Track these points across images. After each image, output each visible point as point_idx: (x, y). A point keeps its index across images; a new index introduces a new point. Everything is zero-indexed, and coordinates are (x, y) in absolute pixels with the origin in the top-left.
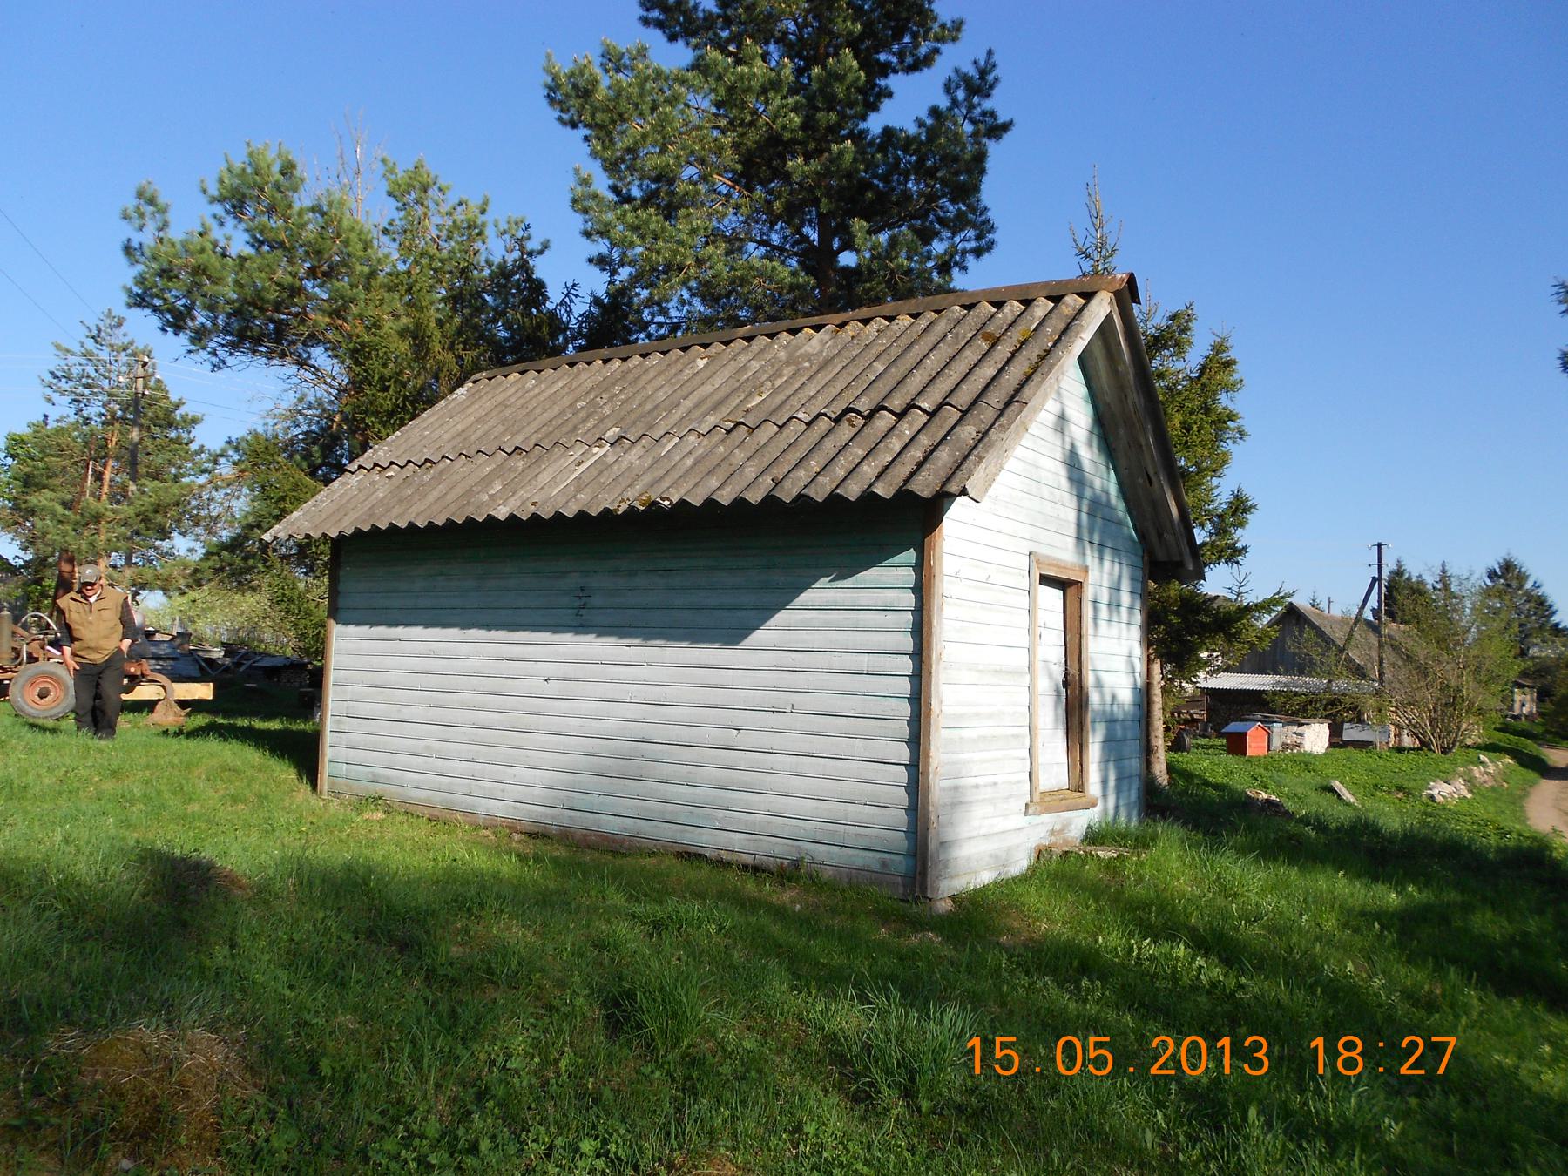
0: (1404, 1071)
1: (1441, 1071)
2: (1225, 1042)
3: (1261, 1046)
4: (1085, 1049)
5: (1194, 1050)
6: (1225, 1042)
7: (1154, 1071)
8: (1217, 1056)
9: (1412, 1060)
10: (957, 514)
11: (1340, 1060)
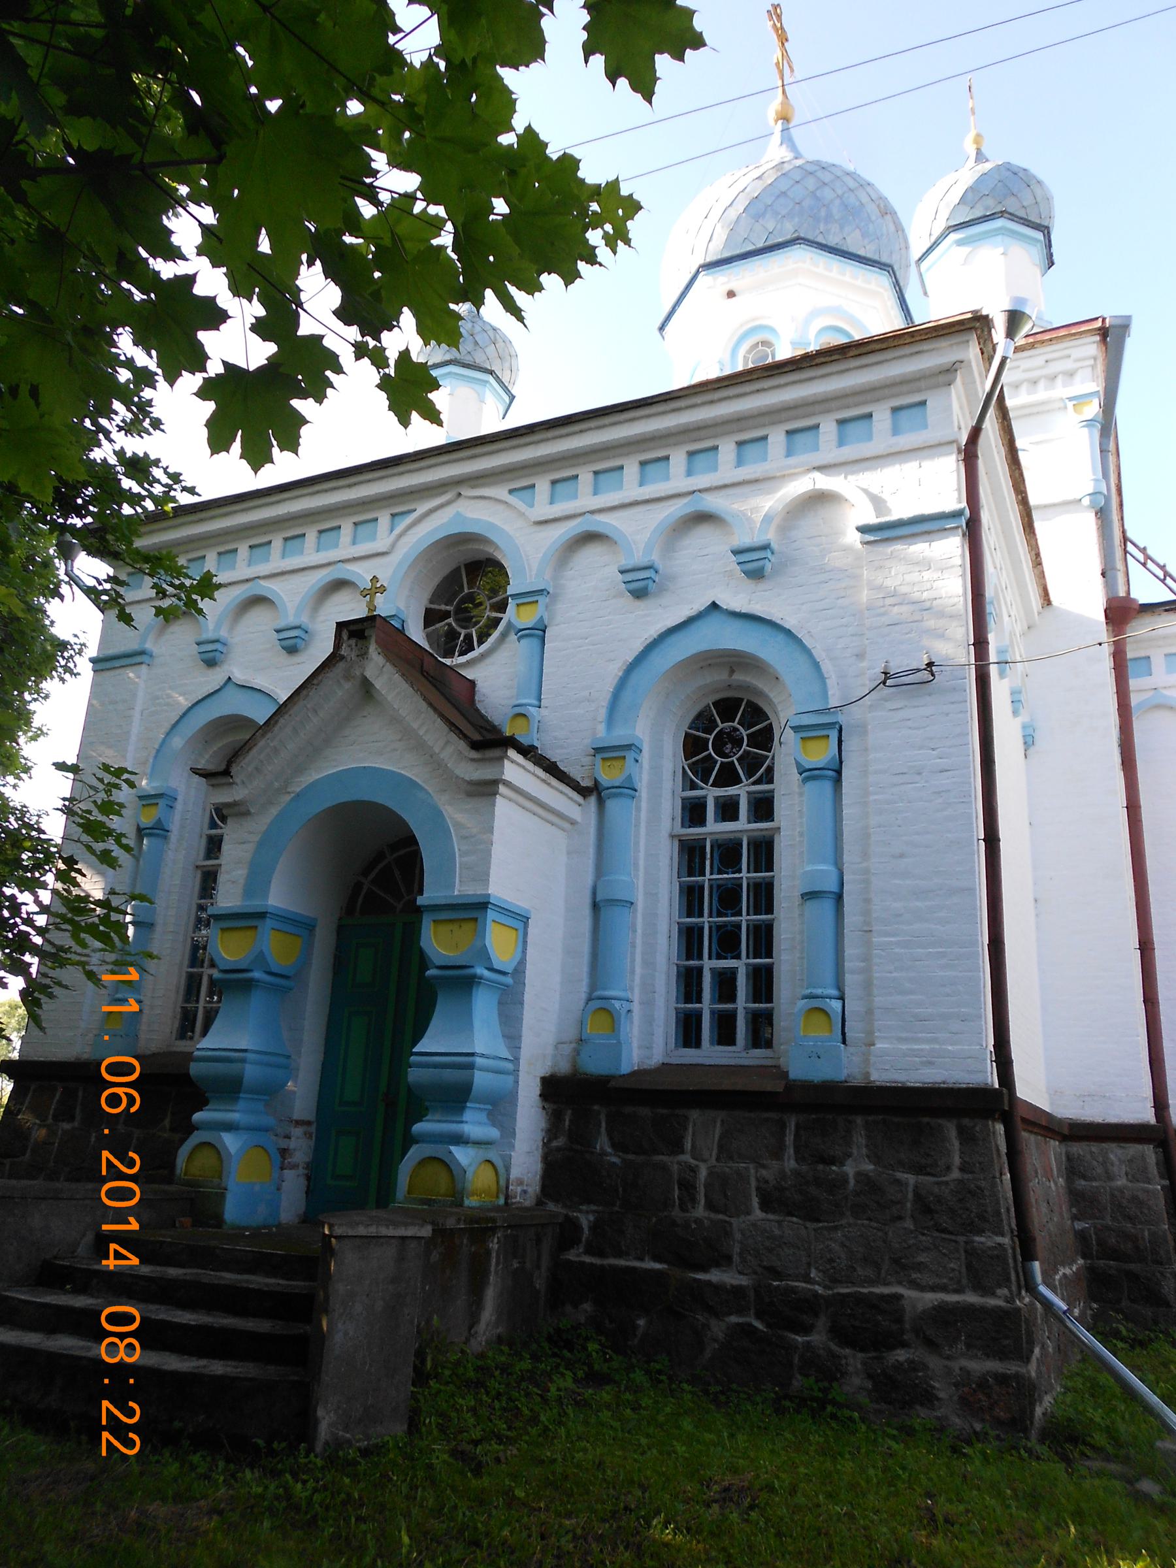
0: (105, 1404)
1: (104, 1453)
2: (134, 1226)
3: (133, 1069)
4: (122, 1336)
5: (126, 1194)
6: (134, 1226)
7: (105, 1404)
8: (120, 1216)
10: (513, 318)
11: (116, 1340)
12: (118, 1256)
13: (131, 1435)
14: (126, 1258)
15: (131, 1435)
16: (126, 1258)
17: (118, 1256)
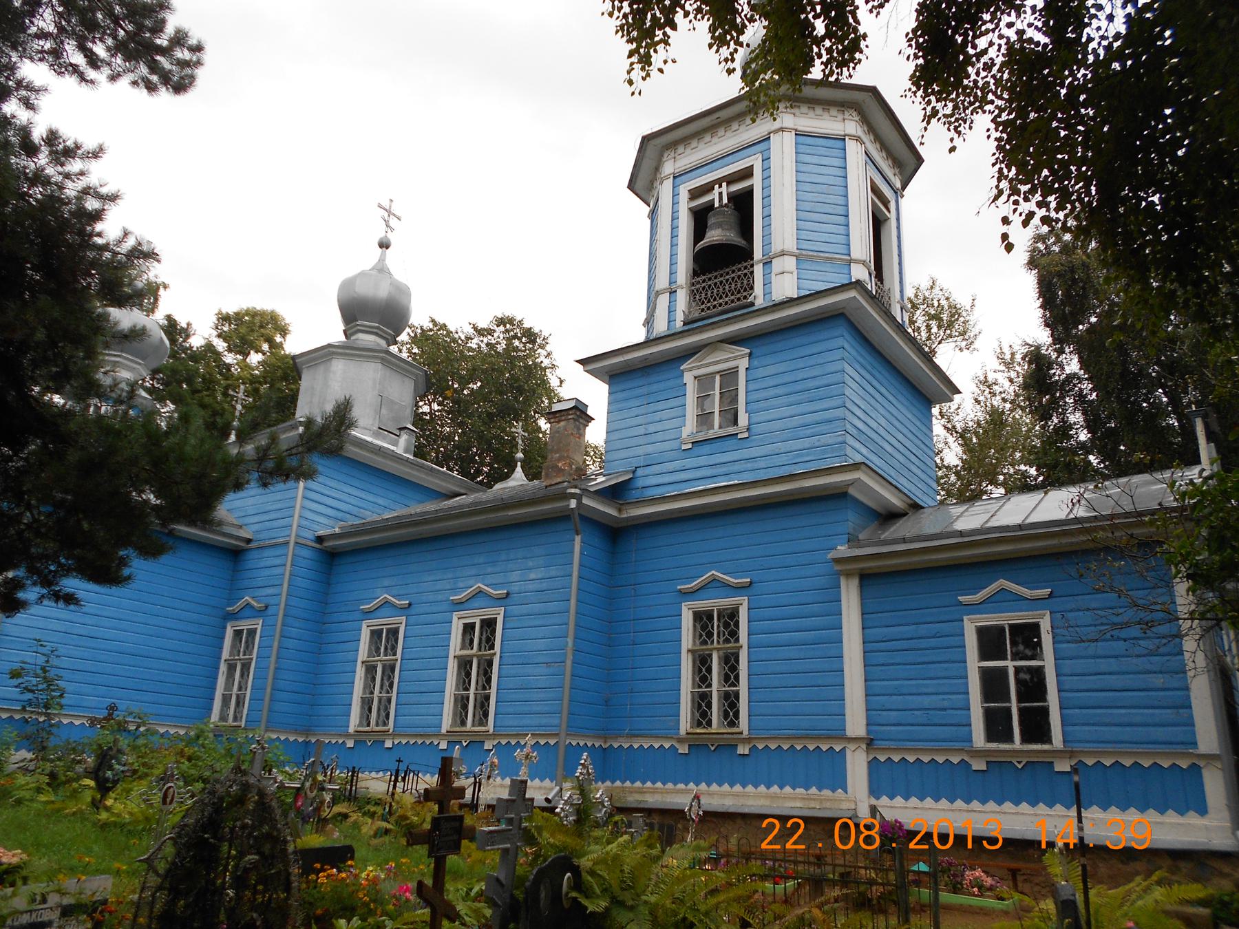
3: (773, 826)
13: (789, 825)
15: (789, 825)
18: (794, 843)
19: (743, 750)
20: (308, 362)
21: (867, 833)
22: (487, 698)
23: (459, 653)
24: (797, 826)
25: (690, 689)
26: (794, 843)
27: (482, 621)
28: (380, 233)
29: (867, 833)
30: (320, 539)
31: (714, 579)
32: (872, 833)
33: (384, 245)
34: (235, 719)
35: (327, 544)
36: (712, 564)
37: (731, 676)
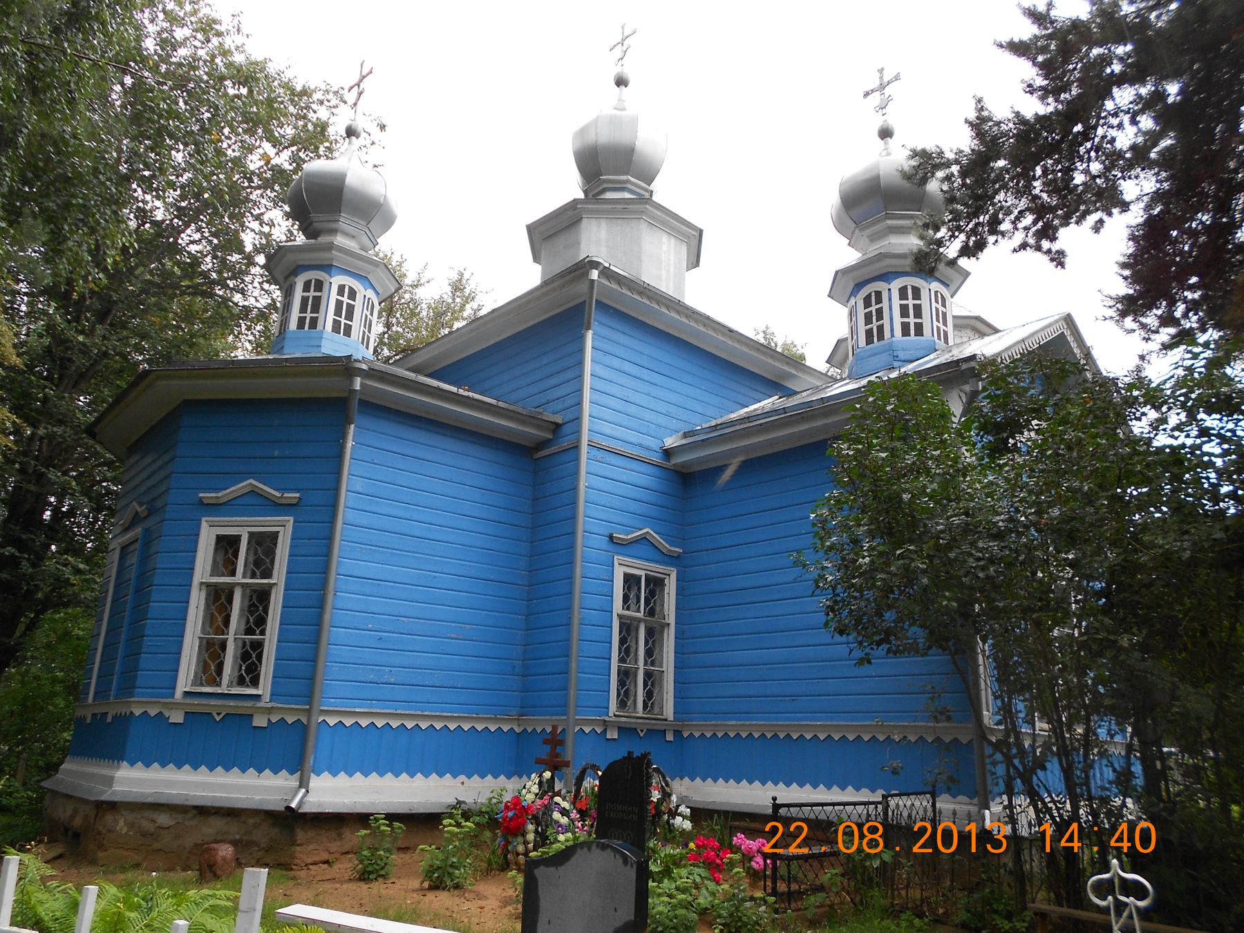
0: (916, 849)
9: (799, 841)
12: (1071, 839)
13: (792, 829)
14: (1122, 833)
15: (792, 829)
16: (1122, 833)
17: (1071, 839)
18: (799, 846)
19: (260, 721)
20: (653, 218)
21: (870, 836)
22: (258, 646)
23: (621, 611)
24: (799, 829)
25: (198, 633)
26: (799, 846)
27: (252, 535)
28: (877, 122)
29: (870, 836)
30: (668, 453)
31: (254, 492)
32: (876, 836)
33: (621, 82)
34: (622, 704)
35: (674, 461)
36: (250, 475)
37: (256, 621)
